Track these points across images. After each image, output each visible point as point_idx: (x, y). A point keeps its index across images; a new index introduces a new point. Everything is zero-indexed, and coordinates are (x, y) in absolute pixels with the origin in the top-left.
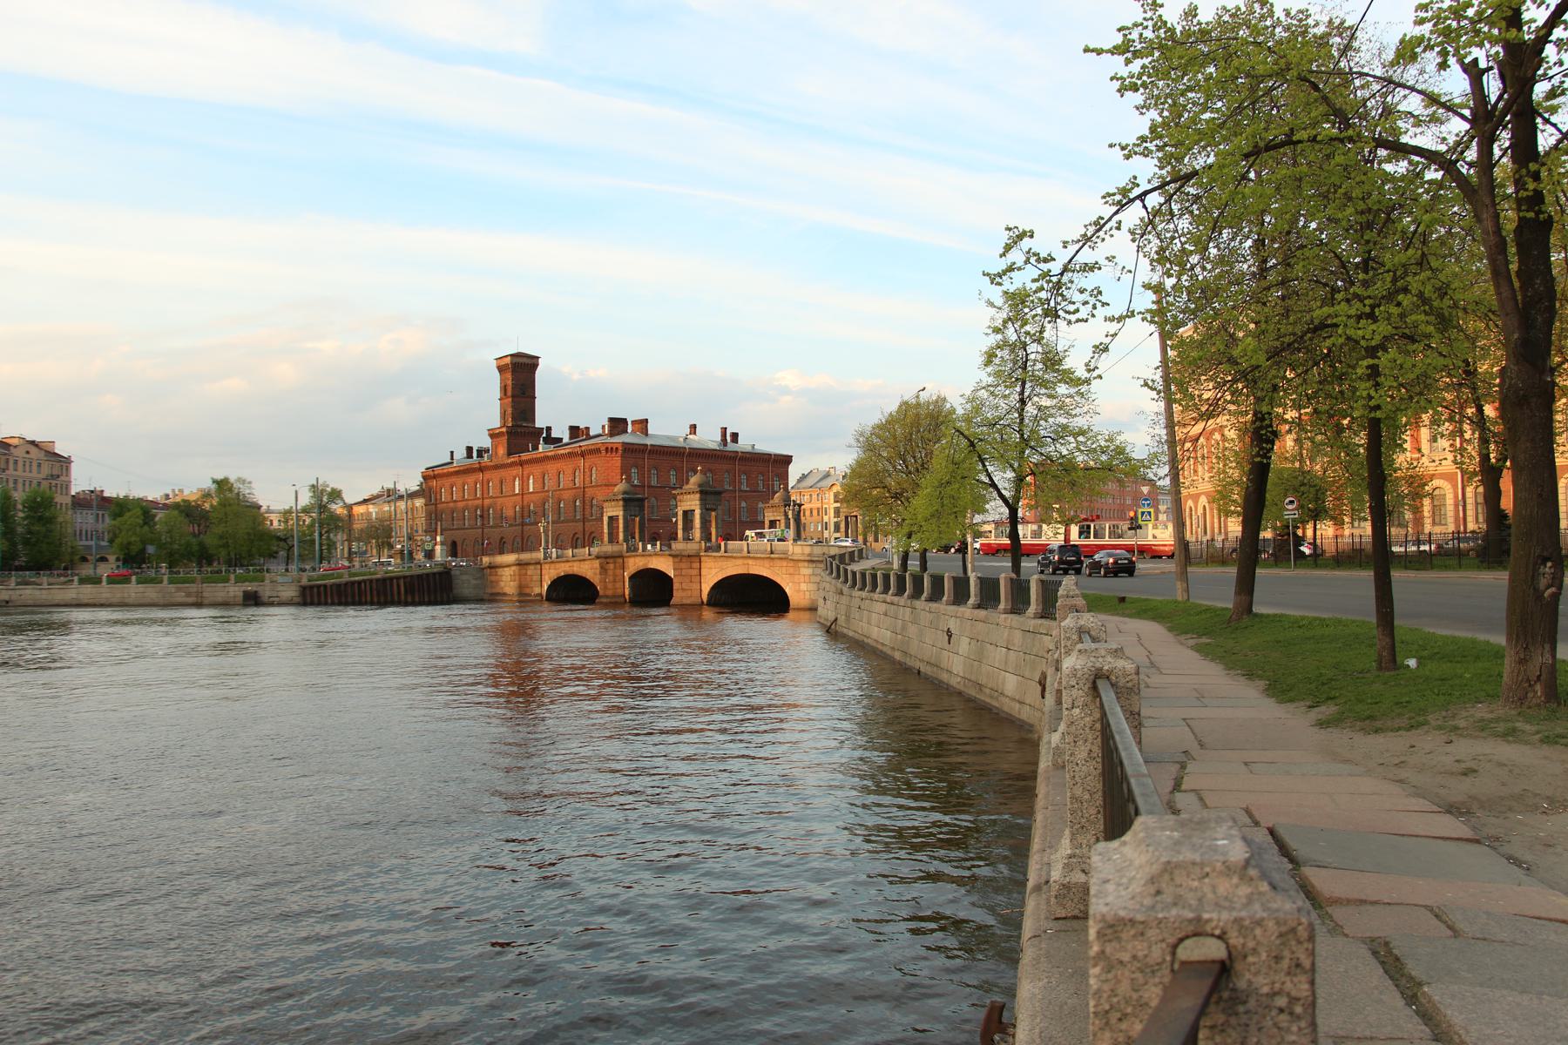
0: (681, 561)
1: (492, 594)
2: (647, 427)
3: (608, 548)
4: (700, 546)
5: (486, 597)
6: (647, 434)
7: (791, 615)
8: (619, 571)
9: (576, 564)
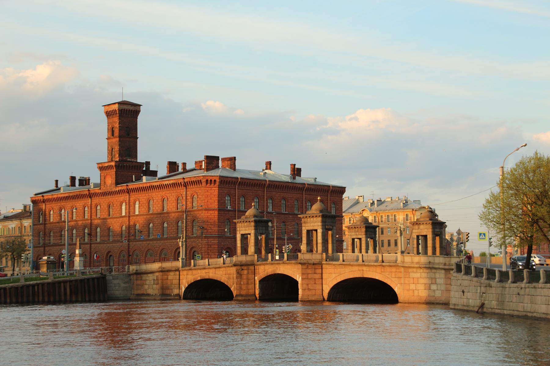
0: (307, 268)
1: (138, 295)
2: (235, 163)
3: (243, 259)
4: (322, 257)
5: (132, 297)
6: (235, 169)
7: (399, 304)
8: (251, 276)
9: (211, 271)
